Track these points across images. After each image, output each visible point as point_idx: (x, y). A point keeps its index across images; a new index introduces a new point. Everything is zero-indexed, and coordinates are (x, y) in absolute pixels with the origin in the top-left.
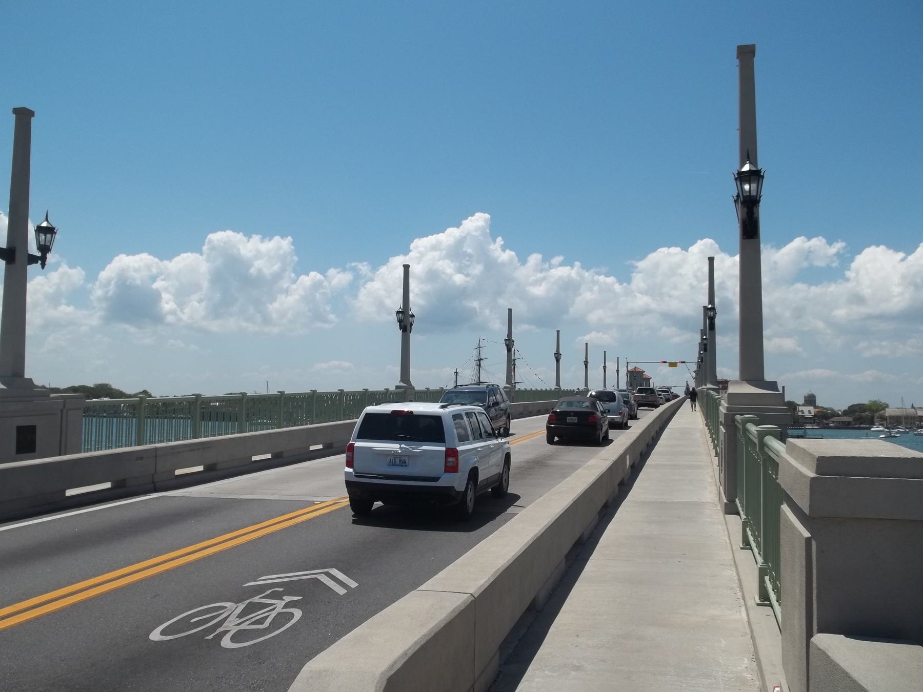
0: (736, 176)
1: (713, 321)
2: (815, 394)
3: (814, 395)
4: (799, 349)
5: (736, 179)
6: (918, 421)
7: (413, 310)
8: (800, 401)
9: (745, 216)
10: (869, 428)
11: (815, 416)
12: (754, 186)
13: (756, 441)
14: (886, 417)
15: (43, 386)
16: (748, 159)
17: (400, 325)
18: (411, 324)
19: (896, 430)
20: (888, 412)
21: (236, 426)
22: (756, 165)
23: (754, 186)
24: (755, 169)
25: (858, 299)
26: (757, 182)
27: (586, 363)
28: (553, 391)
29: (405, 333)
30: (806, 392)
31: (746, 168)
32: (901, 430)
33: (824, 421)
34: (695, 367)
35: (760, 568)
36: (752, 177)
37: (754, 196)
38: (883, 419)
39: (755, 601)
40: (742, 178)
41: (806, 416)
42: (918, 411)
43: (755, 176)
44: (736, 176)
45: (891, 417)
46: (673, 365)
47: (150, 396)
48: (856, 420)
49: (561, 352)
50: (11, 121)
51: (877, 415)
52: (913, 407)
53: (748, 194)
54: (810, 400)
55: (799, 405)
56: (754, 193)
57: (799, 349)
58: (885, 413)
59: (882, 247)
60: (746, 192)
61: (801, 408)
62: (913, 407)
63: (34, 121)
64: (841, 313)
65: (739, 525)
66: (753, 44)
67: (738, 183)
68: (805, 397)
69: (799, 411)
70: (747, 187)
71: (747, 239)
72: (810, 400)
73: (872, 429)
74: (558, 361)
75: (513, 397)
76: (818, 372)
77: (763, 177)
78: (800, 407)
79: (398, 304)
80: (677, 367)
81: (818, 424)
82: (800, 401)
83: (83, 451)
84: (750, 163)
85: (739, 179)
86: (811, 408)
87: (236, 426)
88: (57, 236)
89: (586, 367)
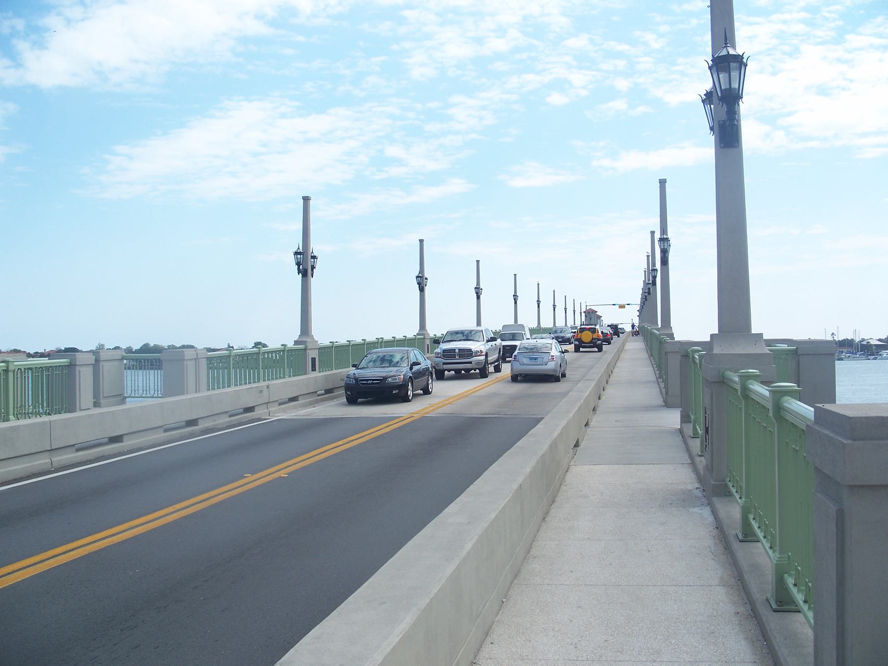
1: (662, 254)
5: (710, 68)
7: (315, 247)
13: (738, 387)
15: (146, 345)
17: (299, 269)
18: (313, 268)
27: (478, 291)
28: (291, 350)
29: (304, 278)
35: (742, 506)
37: (735, 89)
39: (738, 538)
44: (710, 63)
47: (265, 346)
49: (426, 275)
50: (537, 285)
63: (480, 262)
66: (654, 230)
74: (422, 289)
75: (313, 360)
77: (746, 65)
79: (297, 243)
83: (186, 393)
88: (519, 297)
89: (478, 297)
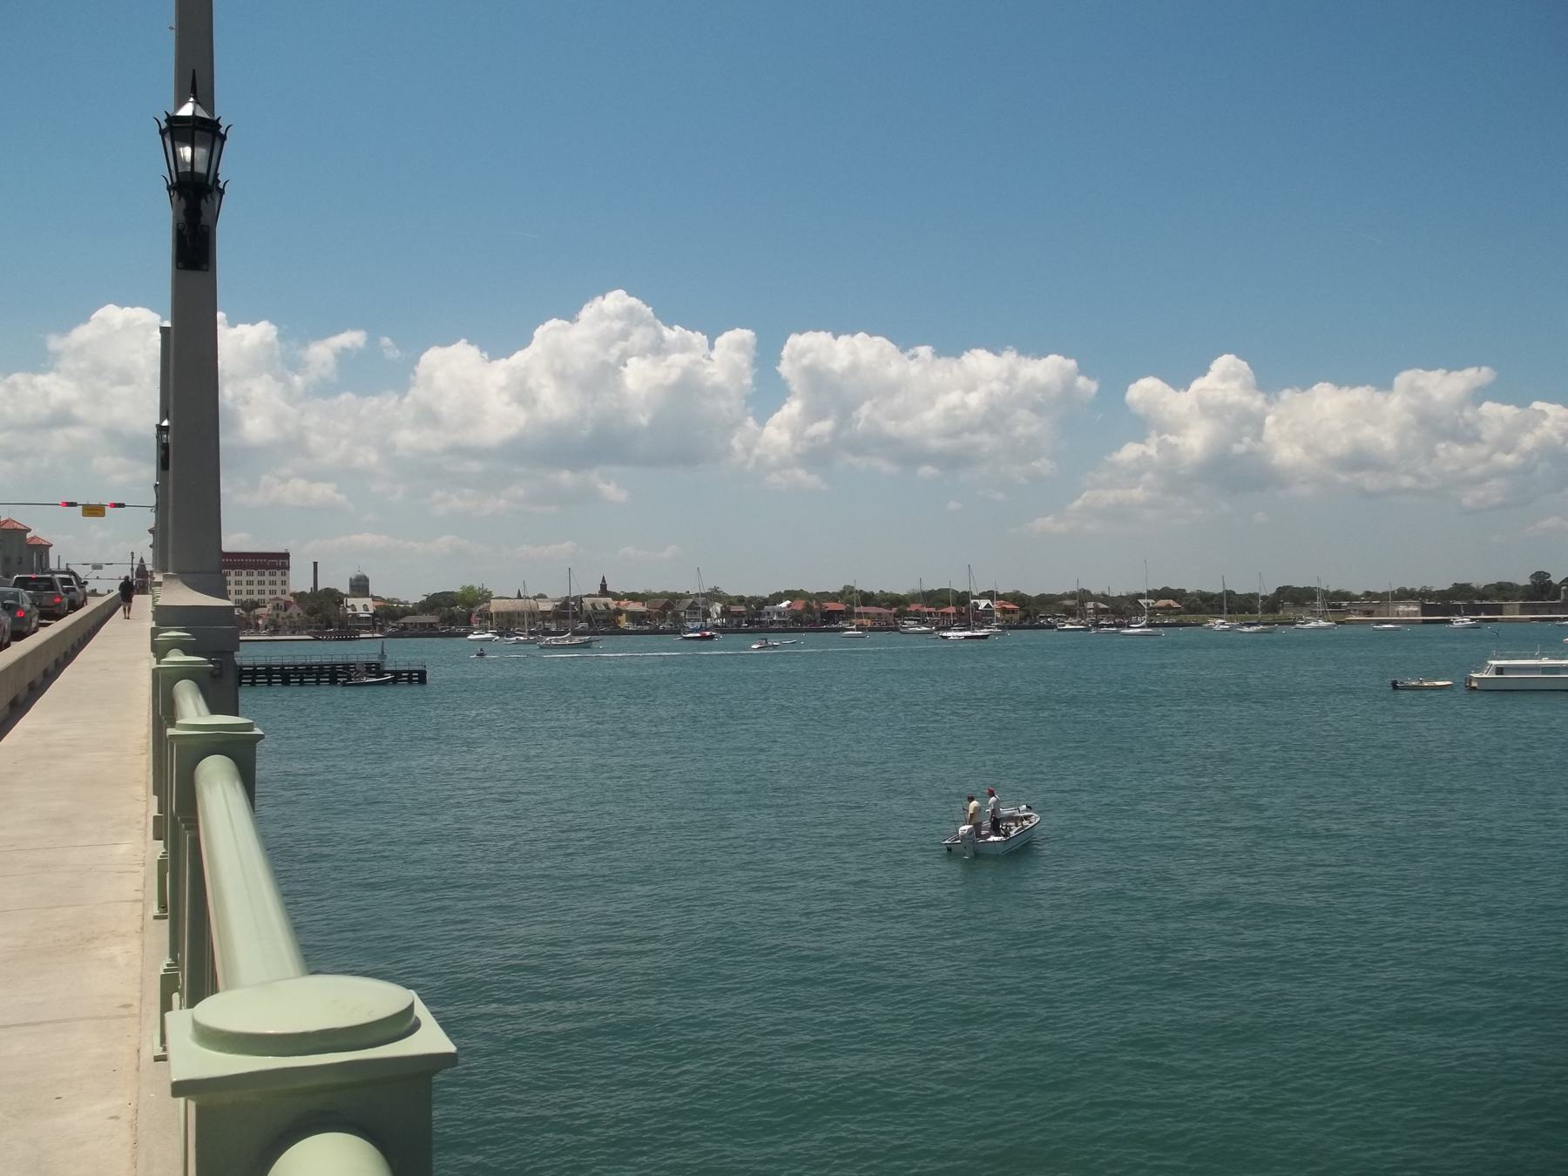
0: (163, 127)
2: (367, 575)
3: (365, 577)
4: (341, 498)
5: (162, 132)
6: (540, 620)
8: (345, 589)
9: (182, 218)
10: (465, 635)
11: (374, 615)
12: (202, 152)
14: (492, 614)
16: (194, 91)
19: (514, 638)
20: (495, 606)
21: (171, 505)
22: (209, 106)
23: (202, 152)
24: (207, 116)
25: (429, 417)
26: (210, 145)
30: (353, 574)
31: (187, 110)
32: (522, 638)
33: (390, 623)
34: (150, 519)
36: (197, 133)
37: (200, 175)
38: (486, 616)
40: (177, 130)
41: (361, 615)
42: (540, 604)
43: (206, 131)
45: (498, 614)
46: (94, 511)
48: (443, 621)
51: (477, 609)
52: (604, 591)
53: (189, 169)
54: (360, 586)
55: (346, 596)
56: (201, 168)
57: (341, 498)
58: (489, 607)
59: (861, 335)
60: (184, 163)
61: (351, 601)
62: (604, 591)
64: (406, 437)
65: (1328, 587)
67: (168, 143)
68: (351, 580)
69: (347, 606)
70: (186, 152)
71: (184, 268)
72: (360, 586)
73: (471, 637)
76: (367, 539)
77: (223, 138)
78: (348, 599)
80: (104, 515)
81: (381, 630)
82: (345, 589)
84: (197, 102)
85: (168, 134)
86: (368, 601)
87: (171, 505)
